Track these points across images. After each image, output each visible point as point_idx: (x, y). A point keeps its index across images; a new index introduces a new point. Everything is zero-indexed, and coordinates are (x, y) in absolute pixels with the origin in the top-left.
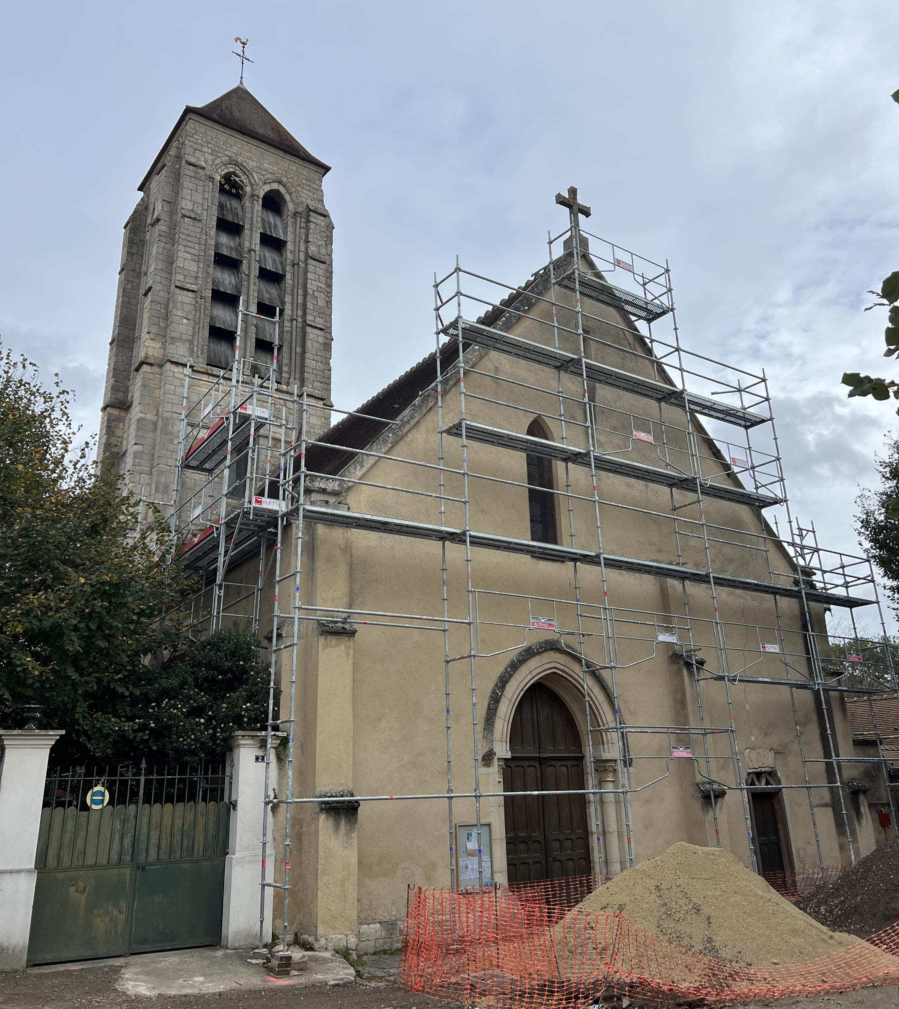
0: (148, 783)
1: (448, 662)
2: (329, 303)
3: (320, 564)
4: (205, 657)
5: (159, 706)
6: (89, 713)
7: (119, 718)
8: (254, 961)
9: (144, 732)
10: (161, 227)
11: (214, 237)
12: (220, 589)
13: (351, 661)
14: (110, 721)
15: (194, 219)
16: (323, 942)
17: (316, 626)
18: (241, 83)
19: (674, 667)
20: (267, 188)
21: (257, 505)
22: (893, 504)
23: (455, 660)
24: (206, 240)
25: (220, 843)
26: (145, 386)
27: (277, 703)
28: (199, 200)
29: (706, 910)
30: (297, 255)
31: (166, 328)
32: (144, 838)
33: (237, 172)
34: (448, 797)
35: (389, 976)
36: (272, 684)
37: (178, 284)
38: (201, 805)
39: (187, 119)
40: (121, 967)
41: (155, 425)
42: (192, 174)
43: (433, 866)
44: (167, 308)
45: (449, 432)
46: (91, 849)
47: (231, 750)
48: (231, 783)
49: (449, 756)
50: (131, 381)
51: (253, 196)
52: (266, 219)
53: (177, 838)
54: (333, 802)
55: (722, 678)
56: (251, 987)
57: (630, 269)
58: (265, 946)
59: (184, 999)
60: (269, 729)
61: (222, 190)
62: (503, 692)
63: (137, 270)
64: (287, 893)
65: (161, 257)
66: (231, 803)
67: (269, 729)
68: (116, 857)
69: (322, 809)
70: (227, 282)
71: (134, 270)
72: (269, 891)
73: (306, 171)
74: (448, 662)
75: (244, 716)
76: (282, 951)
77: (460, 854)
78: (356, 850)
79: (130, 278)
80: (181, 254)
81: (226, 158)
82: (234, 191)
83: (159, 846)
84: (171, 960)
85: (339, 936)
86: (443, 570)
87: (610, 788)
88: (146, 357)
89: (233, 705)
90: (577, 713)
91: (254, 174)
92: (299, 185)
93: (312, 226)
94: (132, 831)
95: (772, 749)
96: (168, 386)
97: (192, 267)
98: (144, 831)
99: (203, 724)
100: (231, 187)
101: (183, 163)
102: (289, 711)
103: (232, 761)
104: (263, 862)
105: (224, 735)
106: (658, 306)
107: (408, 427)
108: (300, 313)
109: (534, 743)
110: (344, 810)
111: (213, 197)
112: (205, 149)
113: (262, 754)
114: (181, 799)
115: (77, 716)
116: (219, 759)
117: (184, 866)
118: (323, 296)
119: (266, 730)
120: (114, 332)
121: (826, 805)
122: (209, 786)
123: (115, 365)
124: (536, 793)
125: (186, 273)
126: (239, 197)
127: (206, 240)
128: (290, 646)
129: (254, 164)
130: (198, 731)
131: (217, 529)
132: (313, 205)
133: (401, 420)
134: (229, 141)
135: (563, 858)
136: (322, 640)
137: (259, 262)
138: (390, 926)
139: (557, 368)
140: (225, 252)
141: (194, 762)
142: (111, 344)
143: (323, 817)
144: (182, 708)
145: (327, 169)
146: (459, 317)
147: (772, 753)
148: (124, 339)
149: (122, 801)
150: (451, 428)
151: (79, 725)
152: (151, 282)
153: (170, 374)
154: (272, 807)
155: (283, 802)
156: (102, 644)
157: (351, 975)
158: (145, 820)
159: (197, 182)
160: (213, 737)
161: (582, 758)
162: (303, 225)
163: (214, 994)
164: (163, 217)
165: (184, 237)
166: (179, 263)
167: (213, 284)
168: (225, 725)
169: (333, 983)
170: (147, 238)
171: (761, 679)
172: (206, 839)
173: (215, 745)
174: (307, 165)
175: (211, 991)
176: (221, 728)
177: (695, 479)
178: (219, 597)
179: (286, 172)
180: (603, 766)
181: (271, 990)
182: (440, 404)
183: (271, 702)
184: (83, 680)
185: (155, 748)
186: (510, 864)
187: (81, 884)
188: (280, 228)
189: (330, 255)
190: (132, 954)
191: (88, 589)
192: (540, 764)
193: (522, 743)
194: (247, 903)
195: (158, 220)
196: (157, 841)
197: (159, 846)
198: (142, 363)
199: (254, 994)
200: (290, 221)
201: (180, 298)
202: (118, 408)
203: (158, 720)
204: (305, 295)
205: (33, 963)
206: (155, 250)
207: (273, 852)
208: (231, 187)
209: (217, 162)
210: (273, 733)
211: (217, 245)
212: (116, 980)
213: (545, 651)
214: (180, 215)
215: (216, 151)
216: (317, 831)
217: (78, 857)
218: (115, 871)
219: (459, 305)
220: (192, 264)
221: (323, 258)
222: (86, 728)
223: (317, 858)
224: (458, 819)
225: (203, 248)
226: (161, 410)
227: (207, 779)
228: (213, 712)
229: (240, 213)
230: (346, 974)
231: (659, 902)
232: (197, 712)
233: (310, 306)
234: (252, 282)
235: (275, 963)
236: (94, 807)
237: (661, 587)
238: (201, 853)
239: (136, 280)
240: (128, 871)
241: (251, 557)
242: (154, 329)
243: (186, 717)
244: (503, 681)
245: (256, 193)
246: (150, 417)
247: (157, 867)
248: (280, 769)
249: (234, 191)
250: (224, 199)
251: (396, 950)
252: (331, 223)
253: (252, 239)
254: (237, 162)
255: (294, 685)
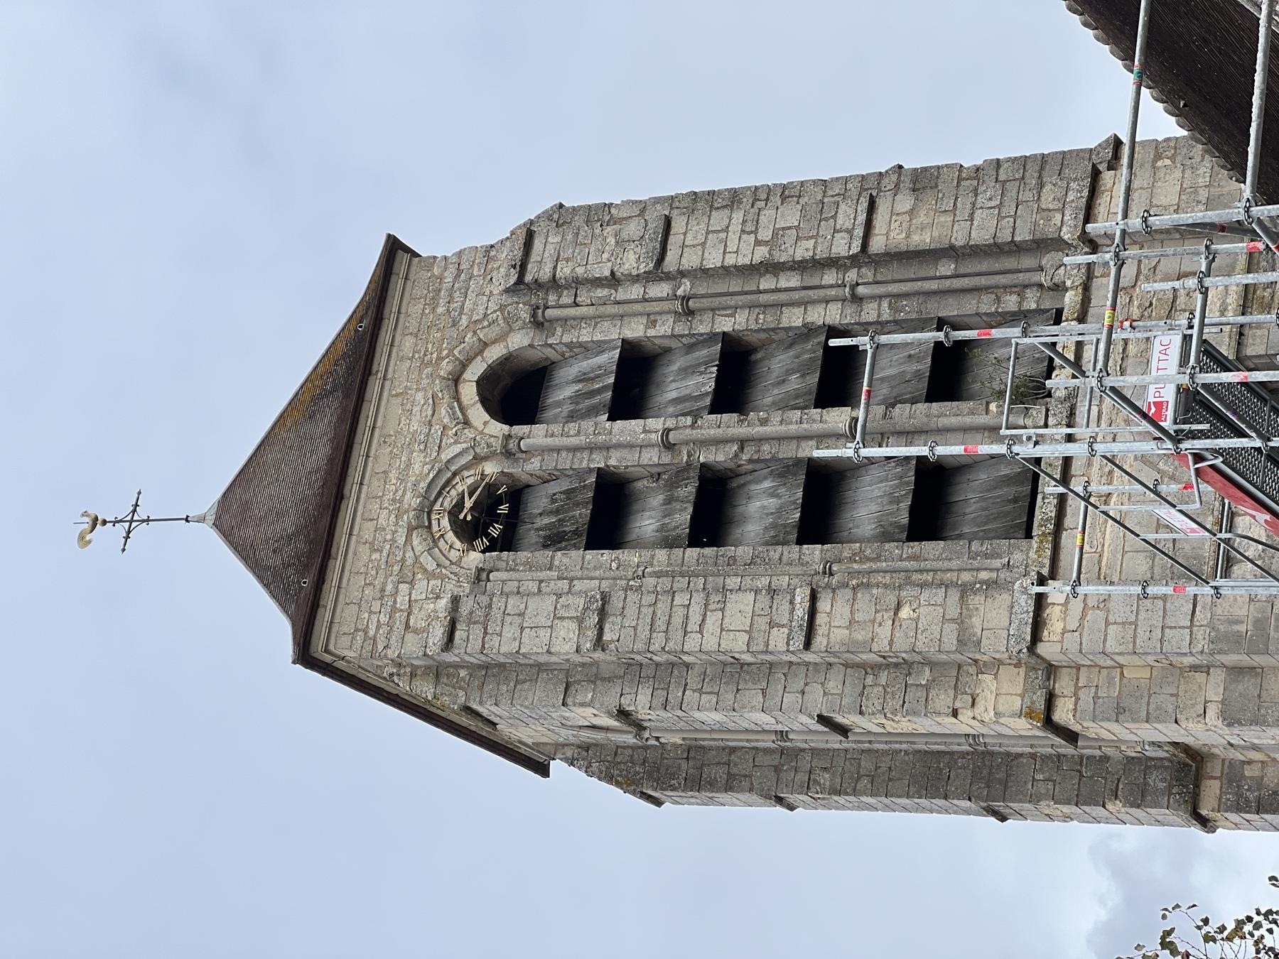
249: (503, 509)
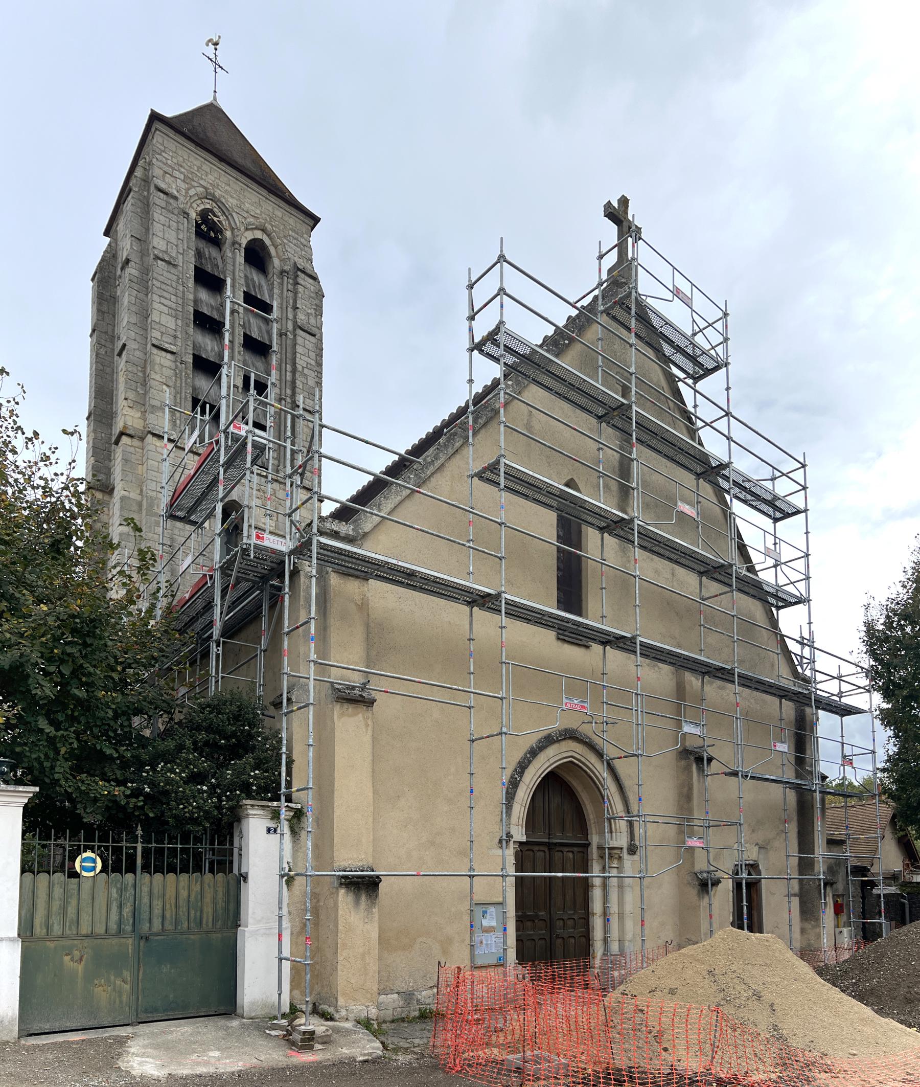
0: (146, 853)
1: (473, 741)
2: (319, 384)
3: (334, 622)
4: (205, 720)
5: (154, 769)
6: (71, 775)
7: (109, 781)
8: (273, 1033)
9: (137, 798)
10: (132, 270)
11: (192, 290)
12: (218, 645)
13: (370, 732)
14: (97, 784)
15: (169, 263)
16: (343, 1013)
17: (330, 692)
18: (215, 99)
19: (683, 763)
20: (250, 236)
21: (259, 542)
22: (905, 613)
23: (482, 738)
24: (183, 292)
25: (232, 916)
26: (126, 461)
27: (289, 773)
28: (172, 238)
29: (768, 997)
30: (284, 322)
31: (145, 394)
32: (145, 908)
33: (215, 210)
34: (469, 876)
35: (414, 1047)
36: (284, 749)
37: (156, 343)
38: (208, 876)
39: (153, 130)
40: (128, 1037)
41: (140, 505)
42: (163, 204)
43: (449, 940)
44: (144, 372)
45: (480, 476)
46: (85, 918)
47: (239, 820)
48: (240, 855)
49: (471, 836)
50: (112, 463)
51: (234, 243)
52: (249, 275)
53: (183, 909)
54: (353, 876)
55: (735, 774)
56: (273, 1064)
57: (687, 302)
58: (284, 1016)
59: (197, 1081)
60: (283, 798)
61: (199, 234)
62: (521, 777)
63: (110, 333)
64: (308, 968)
65: (133, 308)
66: (241, 875)
67: (283, 798)
68: (115, 927)
69: (341, 884)
70: (209, 348)
71: (106, 333)
72: (286, 965)
73: (293, 221)
74: (473, 741)
75: (252, 784)
76: (305, 1024)
77: (475, 929)
78: (376, 925)
79: (103, 342)
80: (156, 306)
81: (202, 189)
82: (212, 234)
83: (163, 917)
84: (182, 1030)
85: (360, 1008)
86: (469, 640)
87: (614, 873)
88: (125, 427)
89: (238, 773)
90: (587, 802)
91: (234, 214)
92: (285, 237)
93: (300, 289)
94: (132, 899)
95: (757, 844)
96: (150, 462)
97: (170, 323)
98: (146, 900)
99: (205, 792)
100: (208, 231)
101: (152, 188)
102: (303, 776)
103: (241, 832)
104: (280, 936)
105: (230, 803)
106: (711, 357)
107: (432, 469)
108: (289, 392)
109: (545, 829)
110: (365, 885)
111: (189, 238)
112: (176, 174)
113: (274, 826)
114: (185, 870)
115: (56, 776)
116: (225, 830)
117: (192, 937)
118: (312, 374)
119: (279, 800)
120: (90, 406)
121: (795, 895)
122: (216, 858)
123: (94, 443)
124: (560, 875)
125: (163, 329)
126: (217, 243)
127: (183, 292)
128: (304, 707)
129: (234, 202)
130: (199, 801)
131: (211, 577)
132: (301, 264)
133: (425, 460)
134: (204, 167)
135: (565, 936)
136: (337, 707)
137: (243, 326)
138: (408, 996)
139: (599, 418)
140: (205, 310)
141: (198, 832)
142: (88, 419)
143: (342, 891)
144: (180, 773)
145: (316, 220)
146: (501, 322)
147: (757, 847)
148: (102, 412)
149: (117, 869)
150: (485, 469)
151: (61, 786)
152: (125, 338)
153: (151, 447)
154: (286, 881)
155: (301, 875)
156: (81, 693)
157: (378, 1048)
158: (145, 889)
159: (170, 215)
160: (219, 807)
161: (588, 845)
162: (290, 287)
163: (233, 1073)
164: (131, 257)
165: (158, 284)
166: (155, 316)
167: (194, 349)
168: (231, 793)
169: (361, 1058)
170: (118, 294)
171: (768, 777)
172: (215, 911)
173: (221, 814)
174: (294, 211)
175: (229, 1070)
176: (226, 796)
177: (731, 565)
178: (218, 656)
179: (271, 218)
180: (614, 853)
181: (296, 1068)
182: (471, 440)
183: (284, 769)
184: (59, 733)
185: (151, 815)
186: (519, 940)
187: (77, 954)
188: (265, 288)
189: (320, 328)
190: (140, 1023)
191: (51, 620)
192: (549, 849)
193: (534, 828)
194: (261, 976)
195: (127, 261)
196: (161, 912)
197: (163, 917)
198: (122, 434)
199: (278, 1073)
200: (277, 281)
201: (157, 359)
202: (100, 491)
203: (154, 785)
204: (294, 371)
205: (26, 1032)
206: (126, 298)
207: (289, 925)
208: (208, 231)
209: (192, 192)
210: (286, 804)
211: (196, 301)
212: (120, 1054)
213: (564, 739)
214: (152, 256)
215: (190, 176)
216: (336, 907)
217: (70, 926)
218: (114, 941)
219: (502, 306)
220: (168, 318)
221: (314, 330)
222: (69, 790)
223: (337, 932)
224: (477, 898)
225: (180, 301)
226: (144, 488)
227: (213, 850)
228: (216, 779)
229: (220, 265)
230: (373, 1048)
231: (715, 987)
232: (198, 778)
233: (299, 384)
234: (236, 350)
235: (297, 1037)
236: (84, 874)
237: (677, 683)
238: (210, 925)
239: (109, 345)
240: (130, 941)
241: (251, 622)
242: (131, 395)
243: (184, 783)
244: (522, 767)
245: (238, 239)
246: (134, 495)
247: (162, 937)
248: (294, 842)
249: (212, 234)
250: (202, 244)
251: (414, 1018)
252: (321, 290)
253: (232, 296)
254: (214, 196)
255: (311, 749)
